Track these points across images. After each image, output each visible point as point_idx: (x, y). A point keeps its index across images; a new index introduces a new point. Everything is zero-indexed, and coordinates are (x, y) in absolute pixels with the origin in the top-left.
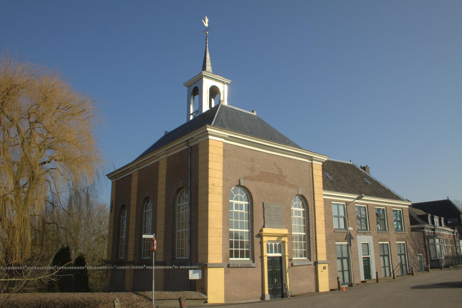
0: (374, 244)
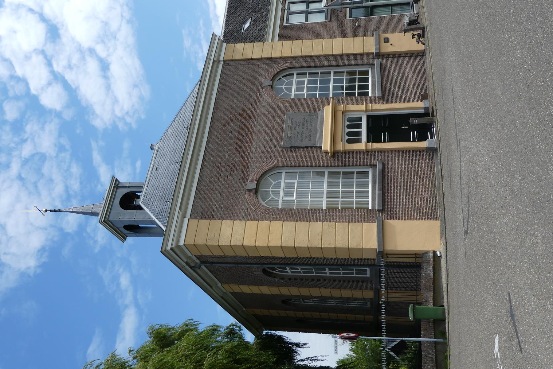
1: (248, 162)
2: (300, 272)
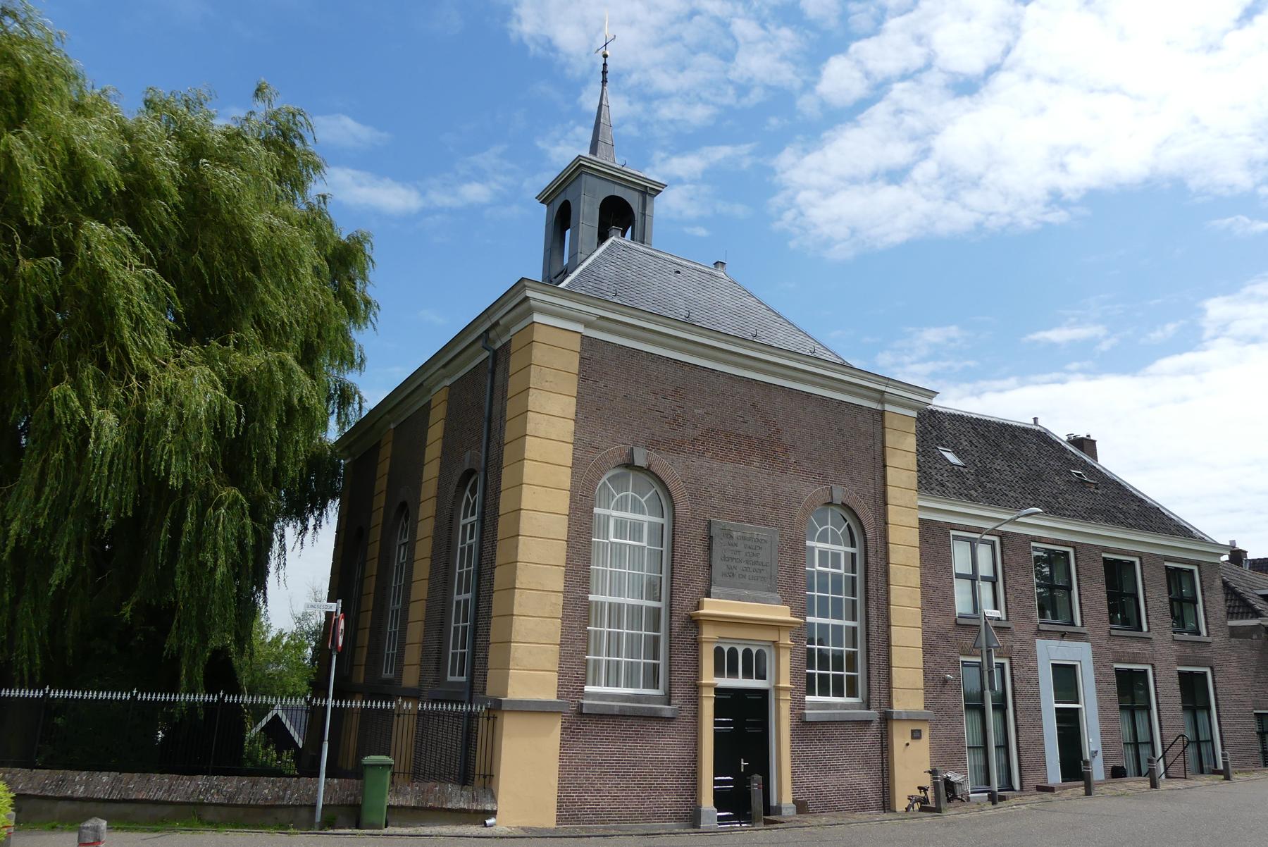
0: (1096, 669)
1: (686, 452)
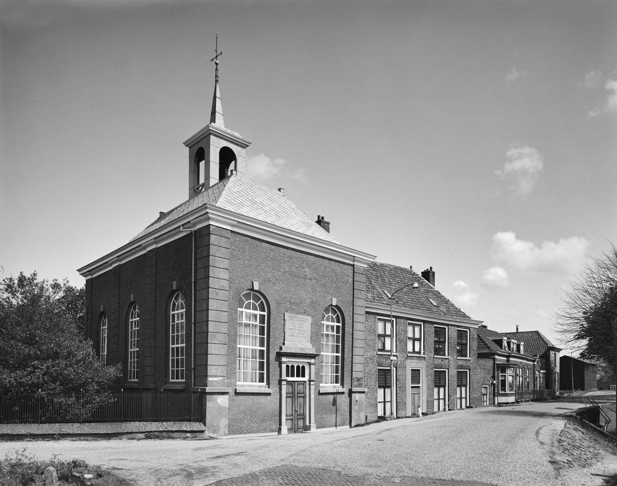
2: (132, 329)
